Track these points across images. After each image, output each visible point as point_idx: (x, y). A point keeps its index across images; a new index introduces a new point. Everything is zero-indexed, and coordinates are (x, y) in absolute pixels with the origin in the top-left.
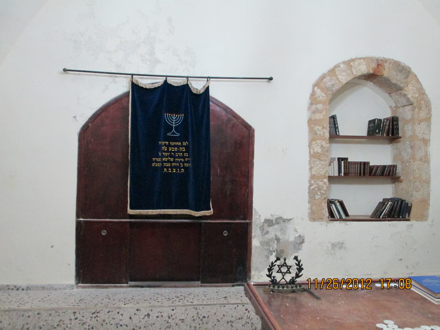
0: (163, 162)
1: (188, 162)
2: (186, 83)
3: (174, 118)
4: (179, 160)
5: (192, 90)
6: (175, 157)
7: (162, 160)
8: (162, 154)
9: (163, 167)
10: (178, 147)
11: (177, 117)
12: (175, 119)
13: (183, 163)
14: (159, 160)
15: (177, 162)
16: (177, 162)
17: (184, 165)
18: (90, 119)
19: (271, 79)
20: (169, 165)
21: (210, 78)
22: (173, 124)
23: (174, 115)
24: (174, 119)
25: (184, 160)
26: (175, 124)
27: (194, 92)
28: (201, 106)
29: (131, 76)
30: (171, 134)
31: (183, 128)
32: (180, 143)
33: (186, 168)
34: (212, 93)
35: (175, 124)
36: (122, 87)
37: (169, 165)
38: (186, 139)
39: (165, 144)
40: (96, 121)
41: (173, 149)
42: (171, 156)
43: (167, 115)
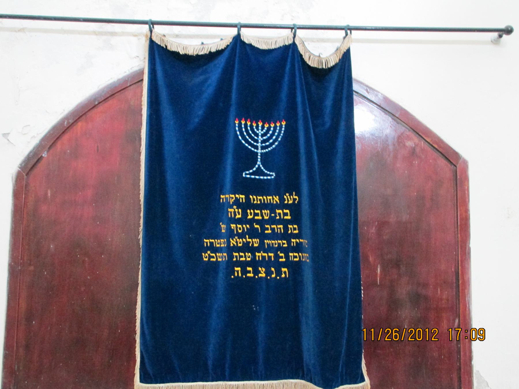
0: (230, 250)
1: (298, 248)
2: (291, 42)
3: (260, 132)
4: (275, 243)
5: (306, 58)
6: (262, 236)
7: (229, 242)
8: (229, 229)
9: (231, 264)
10: (272, 208)
11: (269, 129)
12: (263, 136)
13: (286, 251)
14: (220, 243)
15: (270, 249)
16: (270, 249)
17: (287, 257)
18: (45, 139)
19: (509, 31)
21: (351, 29)
22: (256, 147)
23: (260, 124)
24: (262, 136)
25: (289, 243)
26: (262, 137)
27: (312, 63)
28: (329, 103)
29: (145, 28)
30: (250, 174)
31: (286, 158)
32: (277, 199)
33: (296, 268)
34: (358, 71)
35: (263, 148)
36: (128, 59)
38: (293, 186)
39: (237, 201)
40: (59, 145)
41: (257, 215)
43: (238, 125)
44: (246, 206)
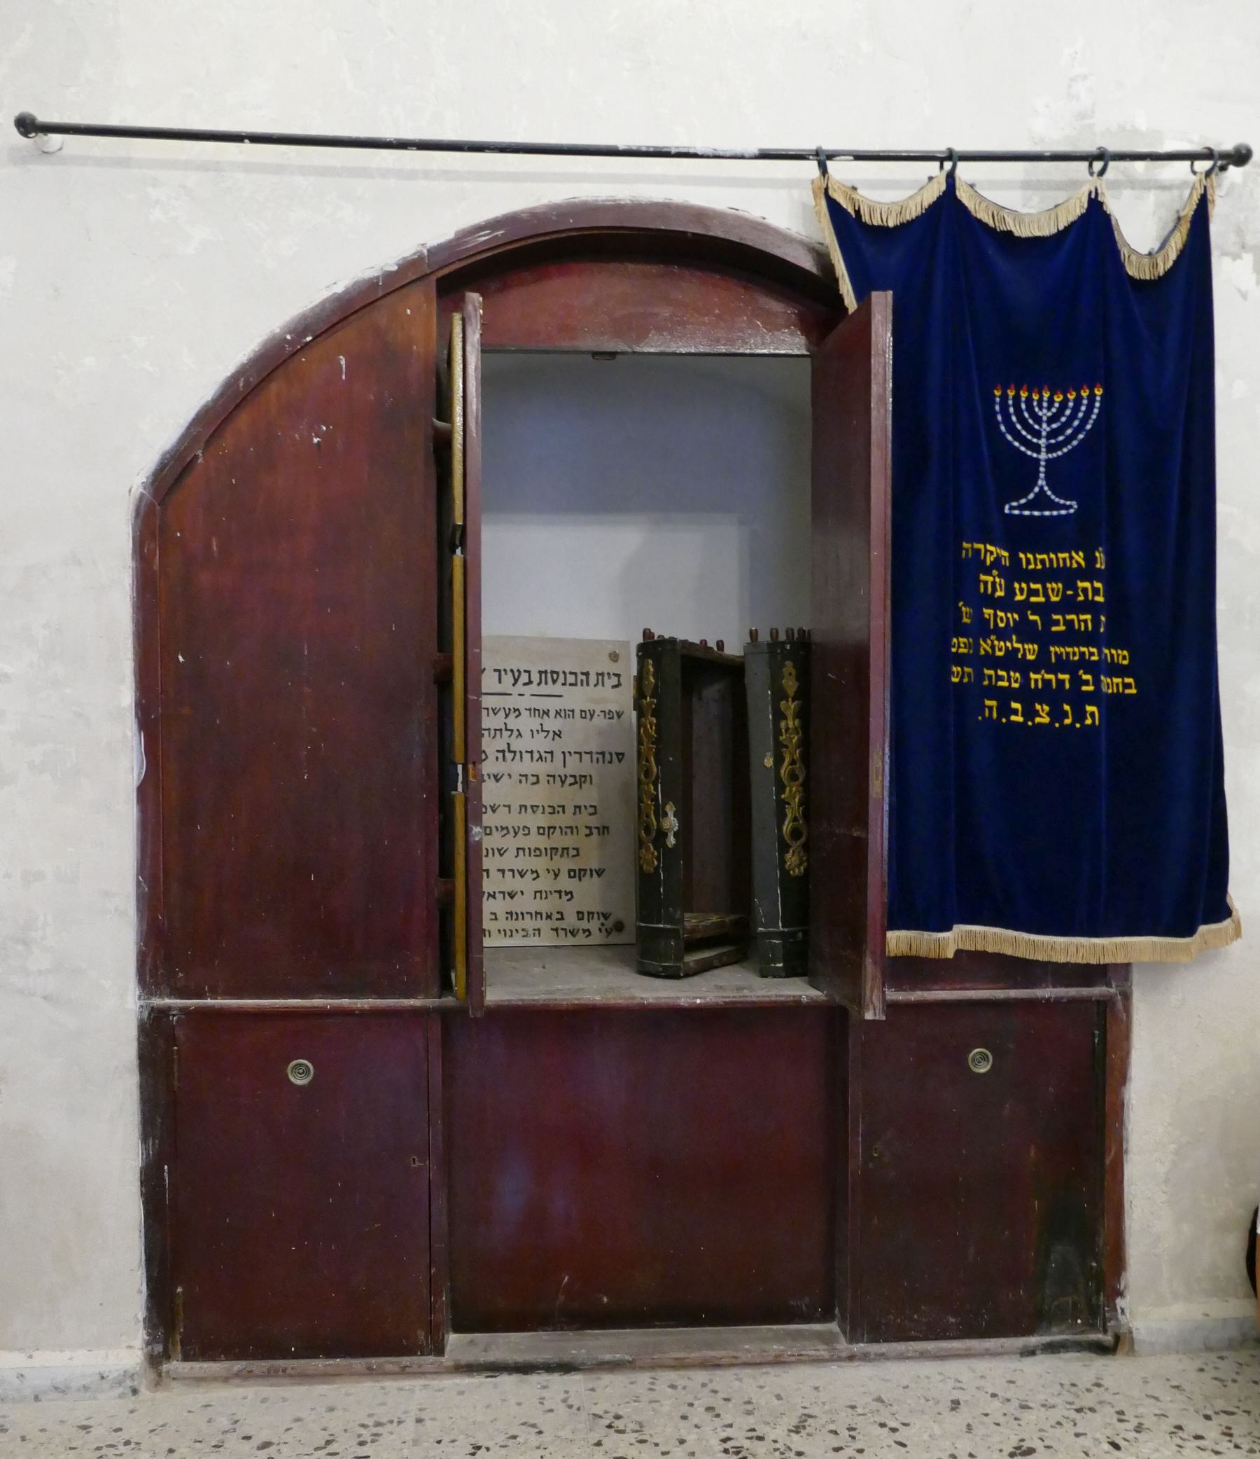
3: (1045, 414)
20: (1012, 680)
37: (1012, 680)
42: (1025, 631)
44: (1014, 573)
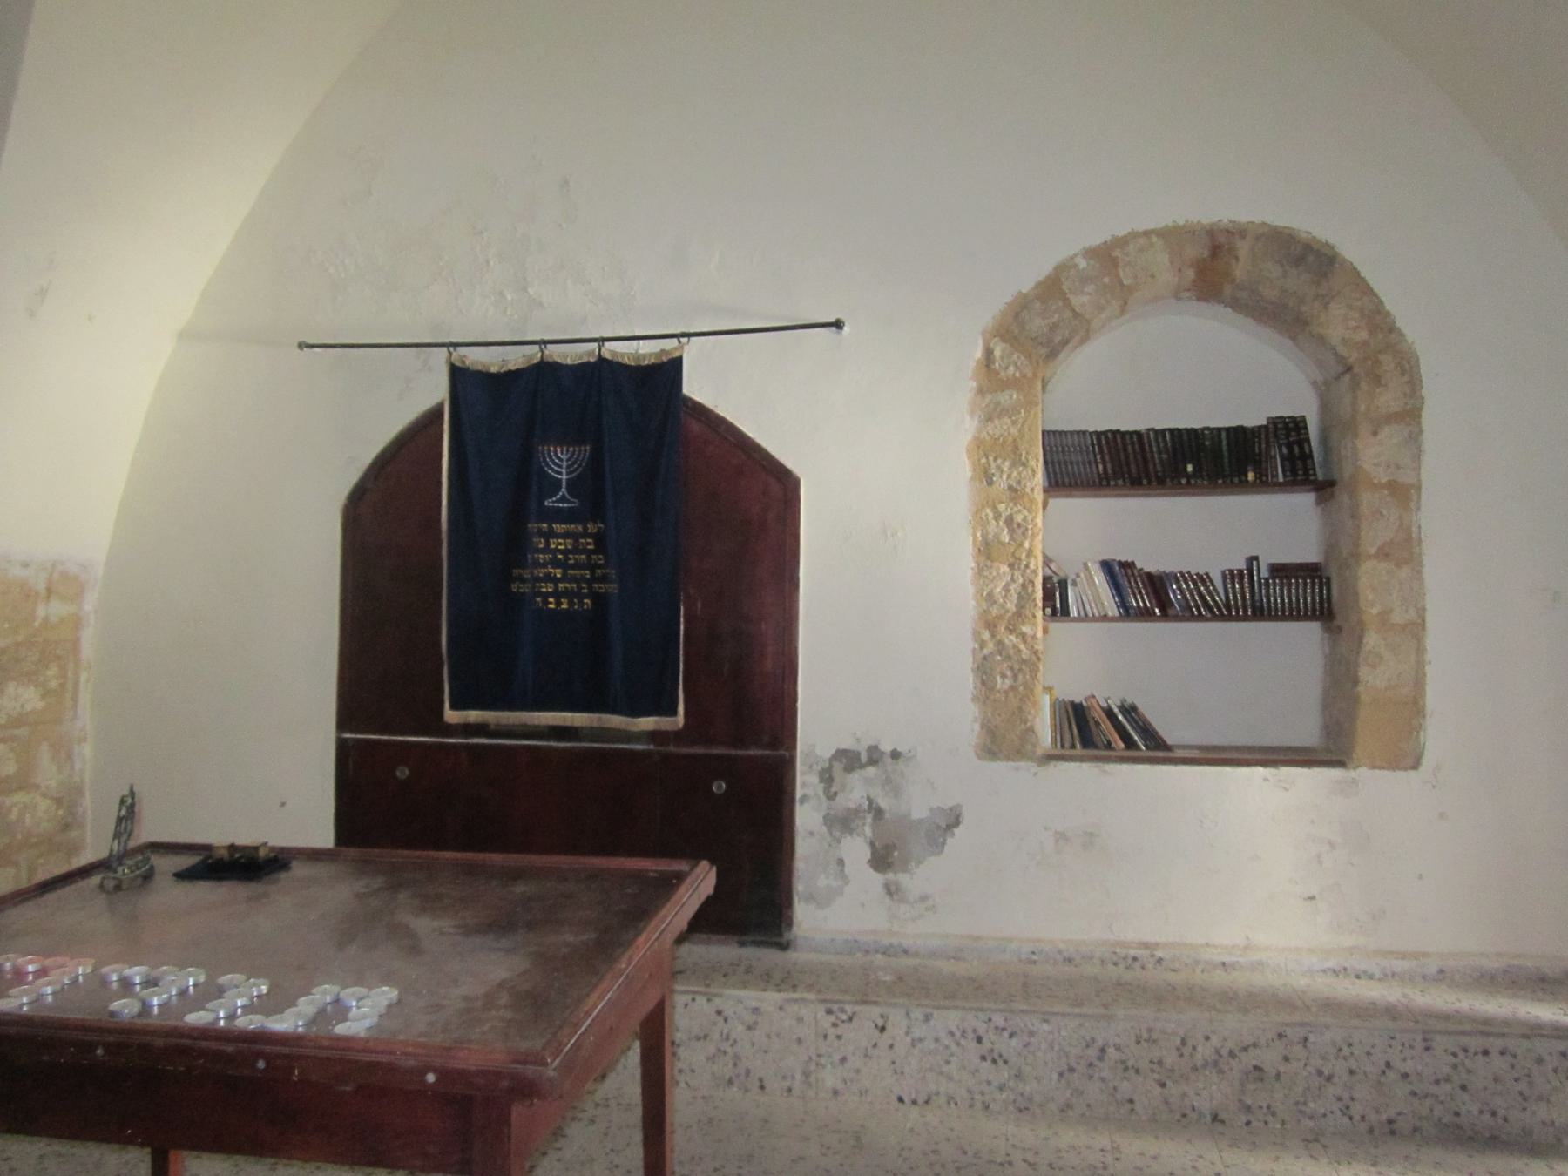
1: (604, 579)
17: (590, 588)
32: (580, 528)
33: (598, 599)
36: (434, 390)
